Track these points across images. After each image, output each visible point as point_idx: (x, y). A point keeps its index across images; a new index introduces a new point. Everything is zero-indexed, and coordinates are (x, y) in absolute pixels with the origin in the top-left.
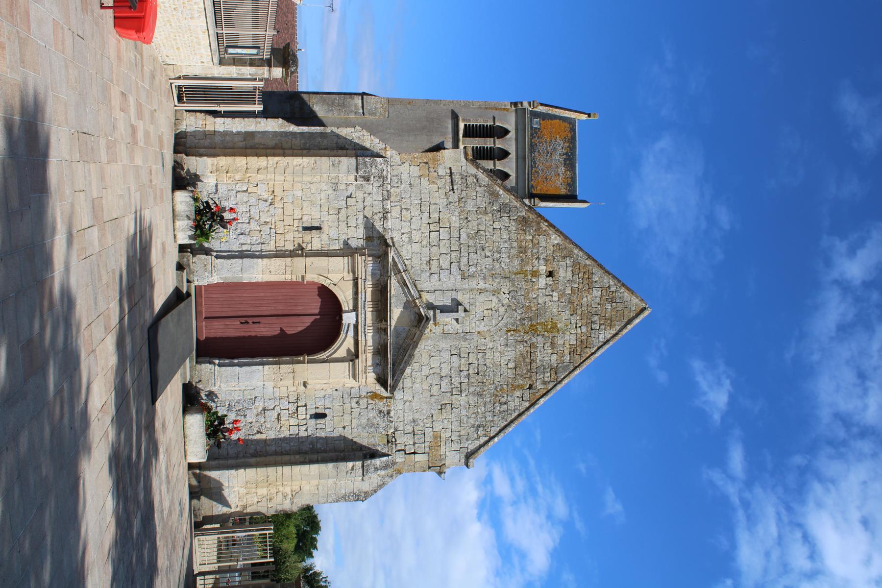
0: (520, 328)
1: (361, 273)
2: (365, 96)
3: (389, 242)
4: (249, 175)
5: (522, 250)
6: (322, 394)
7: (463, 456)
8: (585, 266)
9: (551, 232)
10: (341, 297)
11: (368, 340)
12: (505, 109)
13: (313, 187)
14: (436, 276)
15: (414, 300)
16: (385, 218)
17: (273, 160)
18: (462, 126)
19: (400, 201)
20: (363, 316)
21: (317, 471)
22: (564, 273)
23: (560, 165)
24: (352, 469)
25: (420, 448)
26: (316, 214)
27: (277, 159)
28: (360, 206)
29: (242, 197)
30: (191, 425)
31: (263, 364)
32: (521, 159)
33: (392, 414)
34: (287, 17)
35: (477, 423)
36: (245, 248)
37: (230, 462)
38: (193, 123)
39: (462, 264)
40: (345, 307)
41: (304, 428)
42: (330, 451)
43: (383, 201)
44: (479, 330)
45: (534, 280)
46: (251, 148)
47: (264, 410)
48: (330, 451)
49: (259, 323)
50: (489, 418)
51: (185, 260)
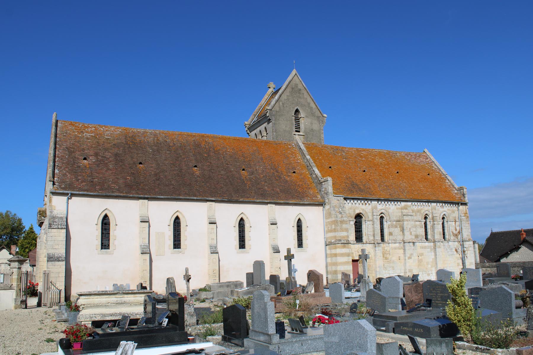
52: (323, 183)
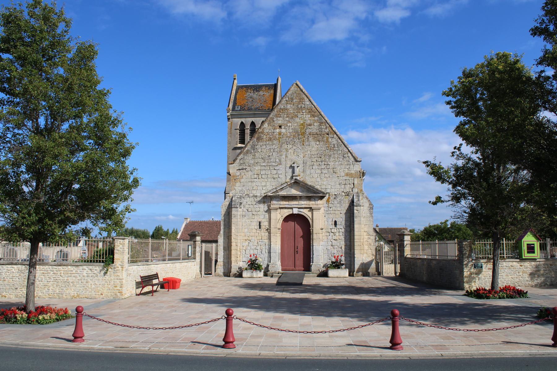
0: (302, 140)
1: (277, 206)
2: (226, 192)
3: (265, 195)
4: (238, 249)
5: (270, 139)
6: (326, 222)
7: (356, 163)
8: (277, 112)
9: (263, 127)
10: (287, 214)
11: (304, 203)
12: (231, 124)
13: (244, 225)
14: (280, 175)
15: (288, 185)
16: (256, 196)
17: (233, 240)
18: (239, 145)
19: (250, 190)
20: (294, 205)
21: (358, 225)
22: (280, 121)
23: (259, 94)
24: (357, 210)
25: (352, 182)
26: (255, 224)
27: (232, 238)
28: (251, 206)
29: (247, 252)
31: (313, 246)
32: (255, 115)
33: (336, 193)
34: (196, 226)
35: (342, 157)
36: (267, 251)
37: (352, 260)
38: (220, 269)
39: (275, 165)
40: (291, 213)
41: (340, 230)
42: (350, 219)
43: (249, 197)
44: (302, 157)
45: (282, 134)
46: (229, 248)
47: (332, 246)
48: (350, 219)
49: (297, 247)
50: (340, 152)
51: (270, 274)
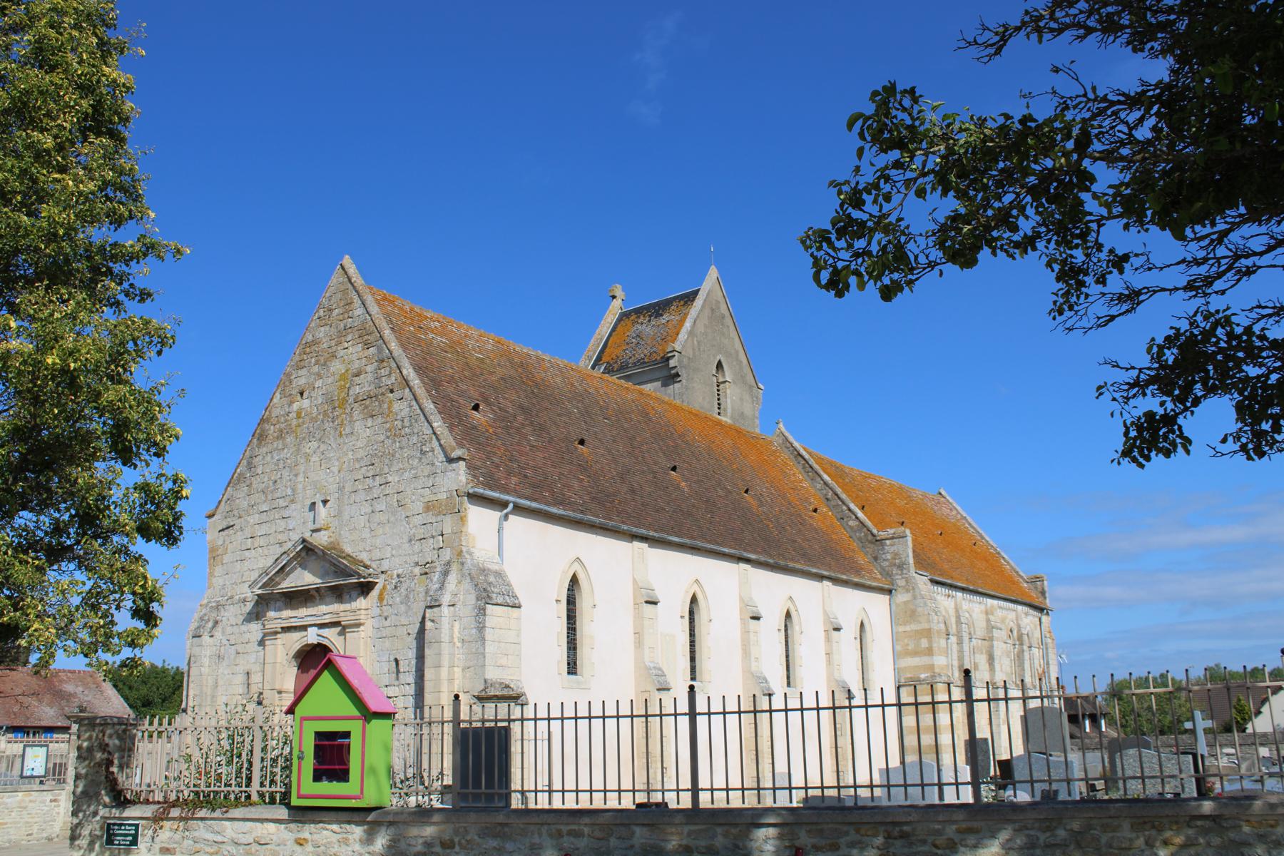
11: (325, 611)
24: (433, 621)
30: (78, 845)
44: (337, 472)
52: (888, 542)
